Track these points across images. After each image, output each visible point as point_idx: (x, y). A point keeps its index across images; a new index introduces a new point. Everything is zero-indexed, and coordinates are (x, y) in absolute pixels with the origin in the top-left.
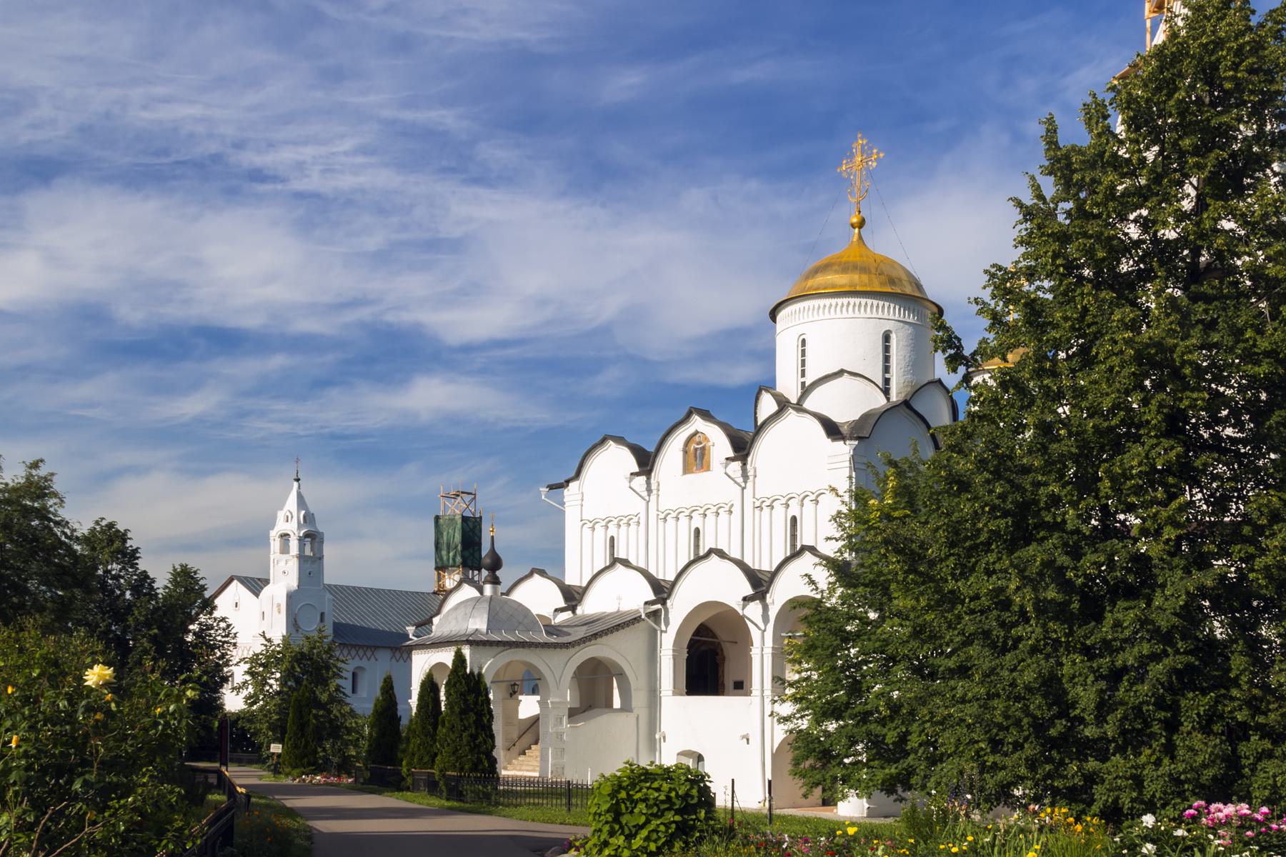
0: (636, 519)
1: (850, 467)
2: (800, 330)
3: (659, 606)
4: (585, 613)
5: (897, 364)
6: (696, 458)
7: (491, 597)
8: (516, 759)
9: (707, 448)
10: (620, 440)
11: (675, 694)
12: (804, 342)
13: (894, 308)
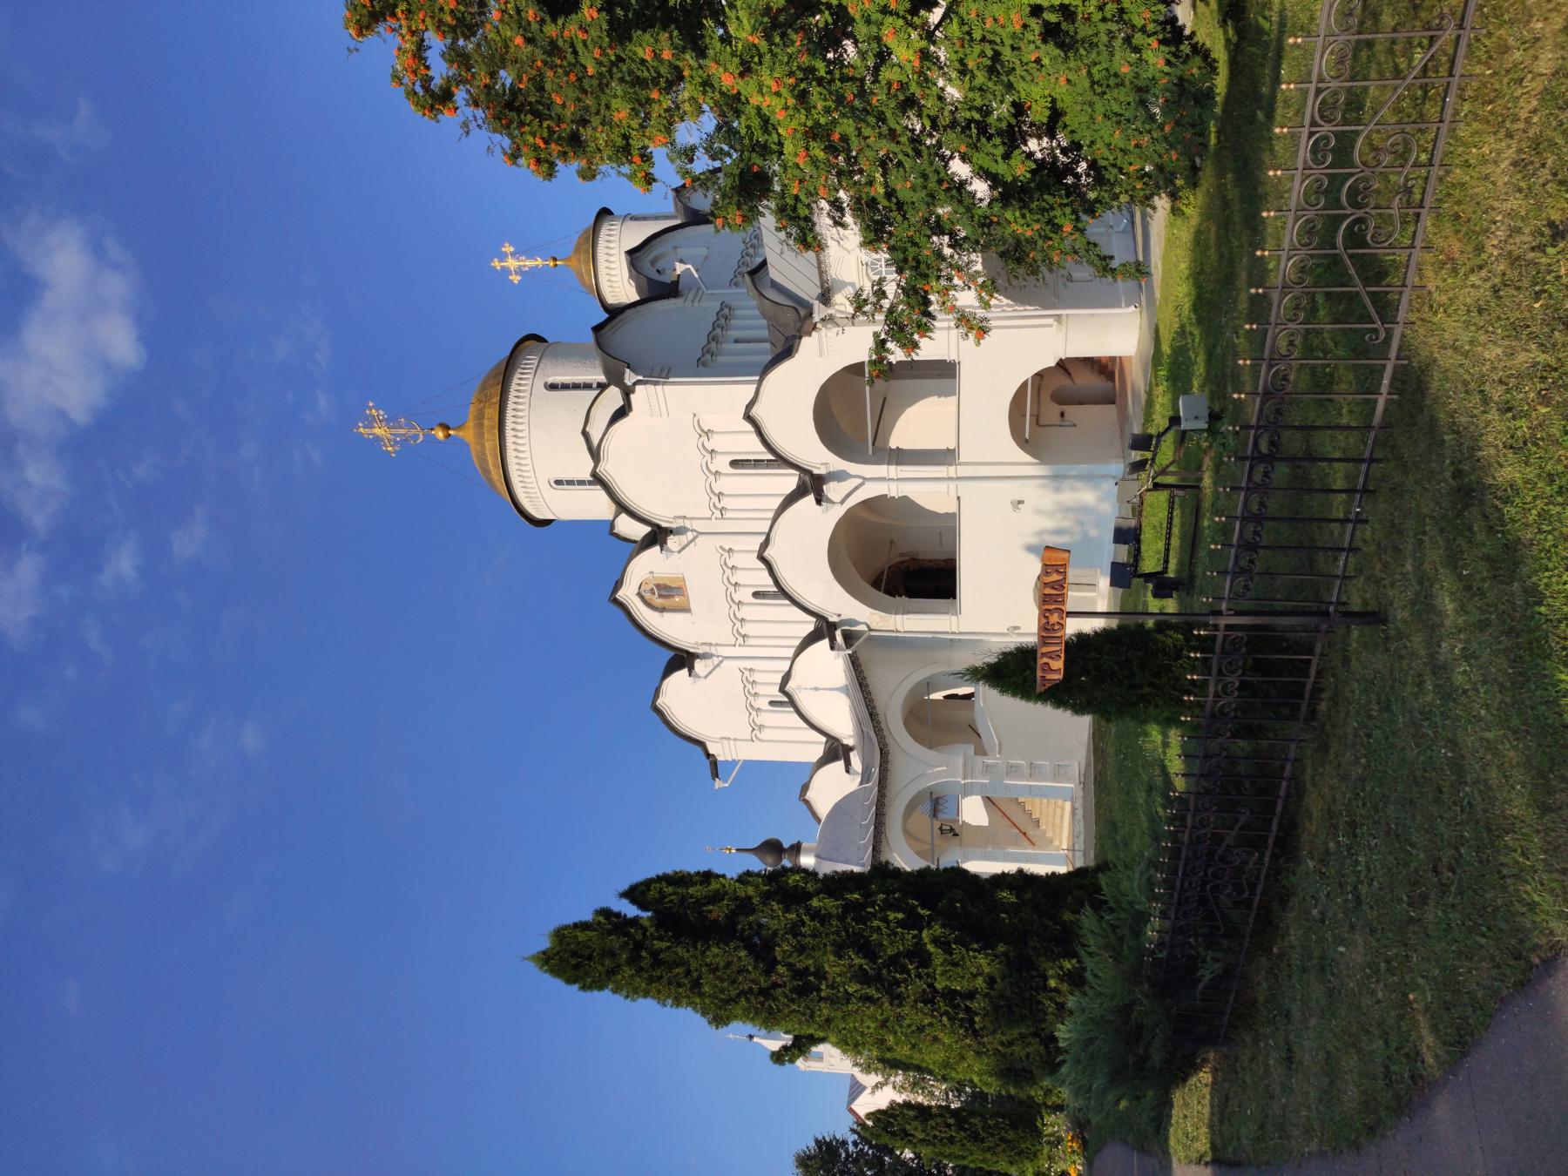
0: (747, 673)
1: (664, 383)
2: (545, 487)
3: (838, 633)
4: (852, 733)
5: (584, 375)
6: (668, 595)
7: (818, 857)
8: (1044, 833)
11: (956, 612)
12: (558, 482)
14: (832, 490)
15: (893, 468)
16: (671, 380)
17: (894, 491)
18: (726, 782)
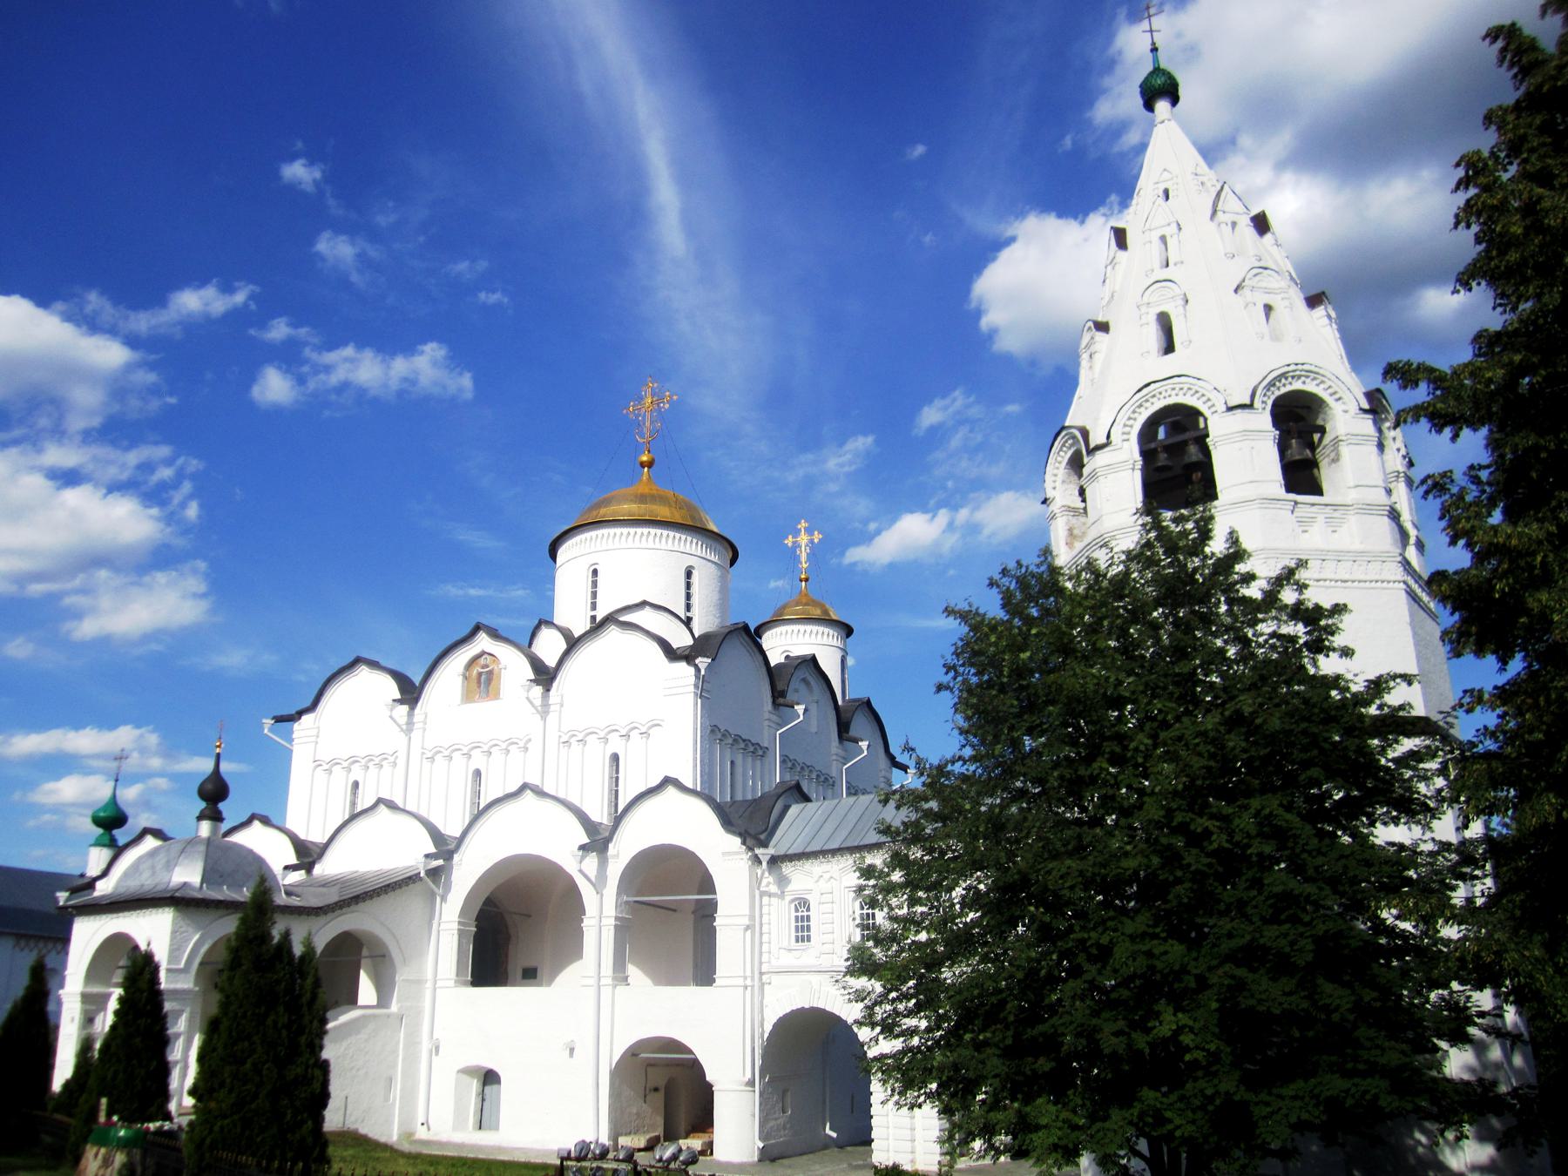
1: (696, 694)
3: (440, 862)
6: (482, 681)
7: (209, 839)
9: (496, 672)
10: (374, 665)
12: (595, 572)
13: (697, 543)
14: (591, 863)
15: (613, 922)
16: (699, 700)
17: (589, 924)
18: (270, 730)
